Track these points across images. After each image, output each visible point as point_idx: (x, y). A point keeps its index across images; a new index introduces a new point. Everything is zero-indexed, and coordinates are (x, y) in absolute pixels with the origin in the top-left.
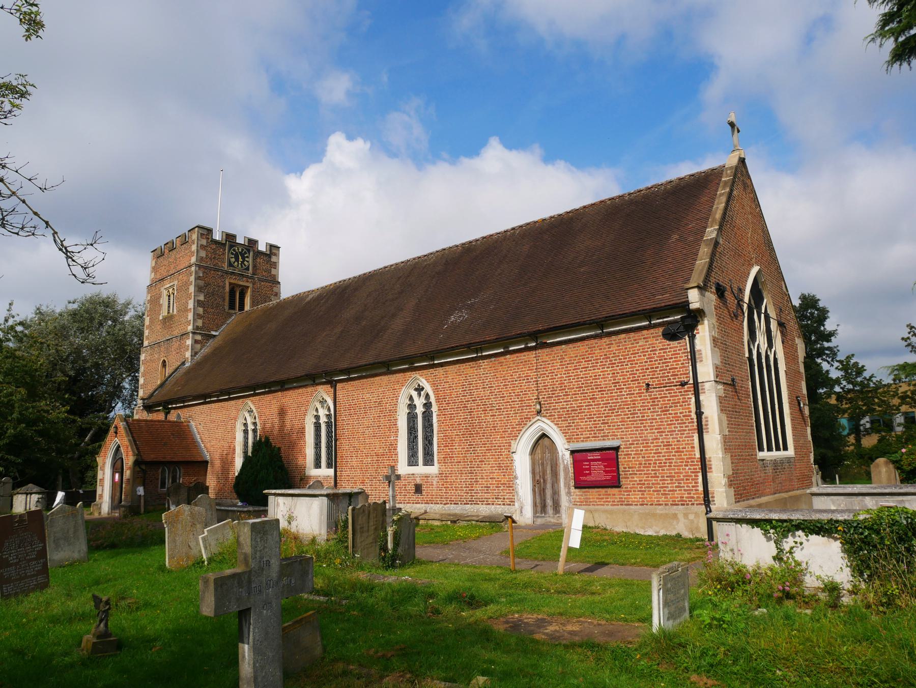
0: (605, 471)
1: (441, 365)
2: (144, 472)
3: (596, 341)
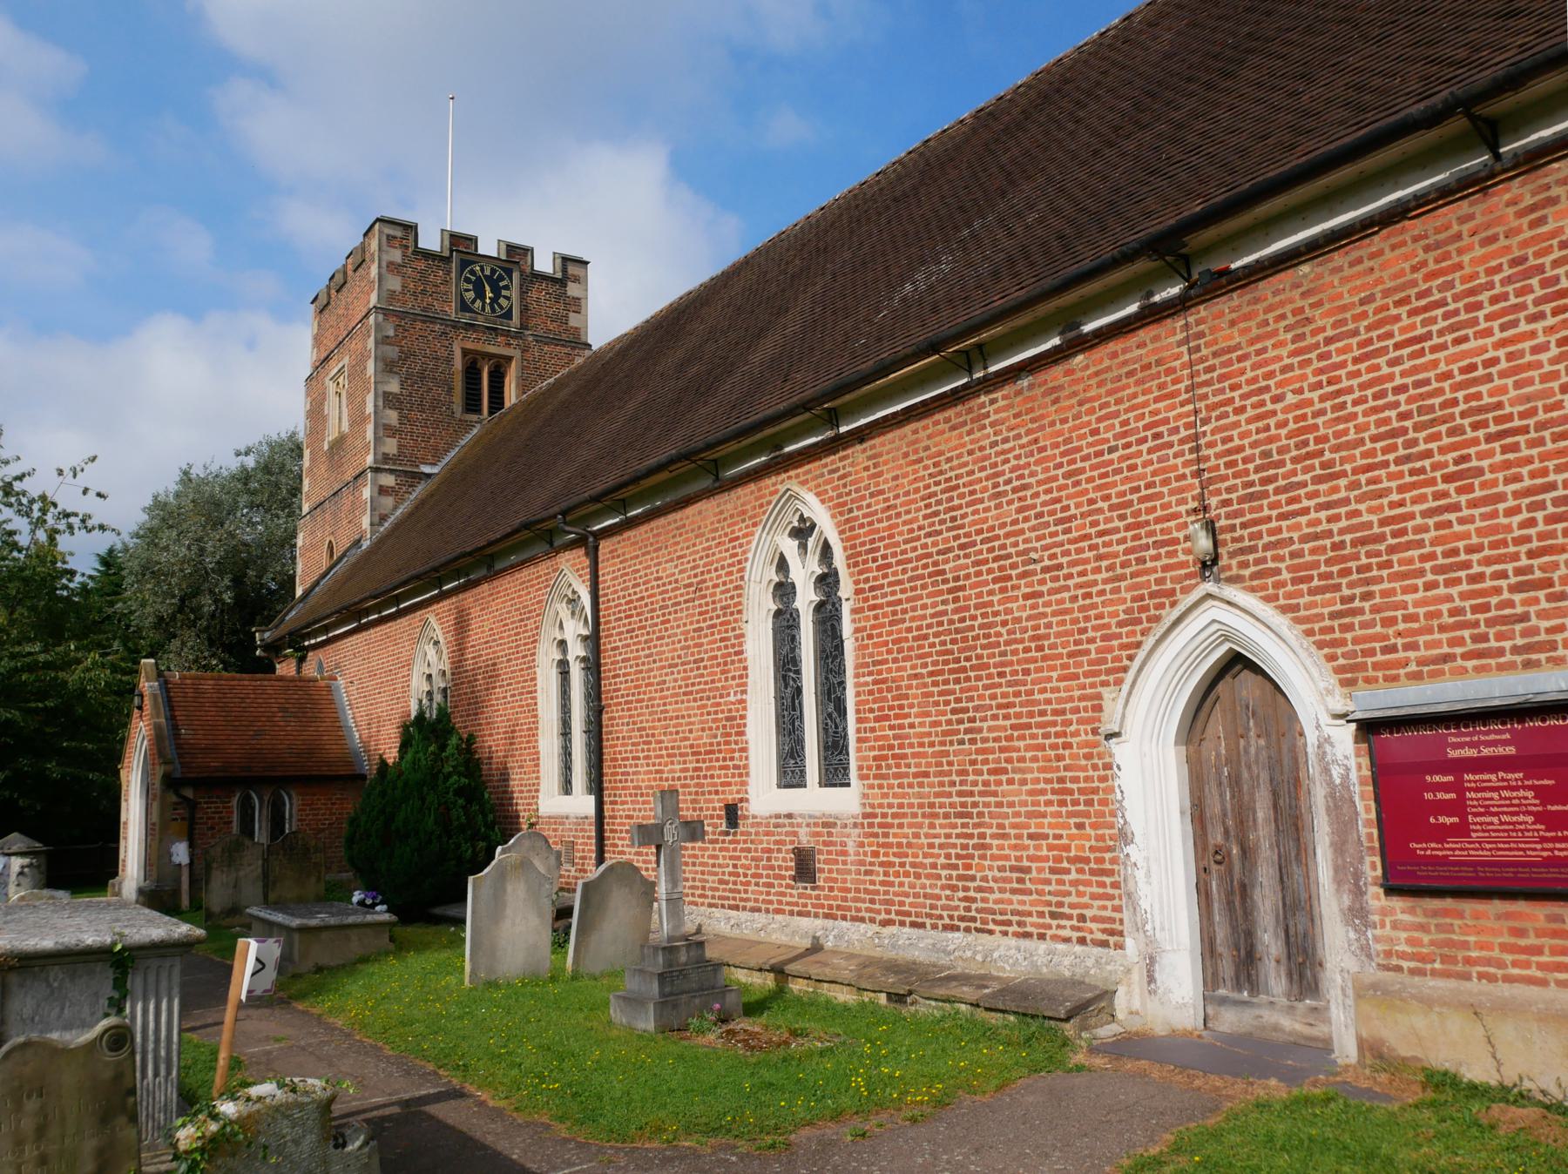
2: (192, 806)
3: (1464, 207)
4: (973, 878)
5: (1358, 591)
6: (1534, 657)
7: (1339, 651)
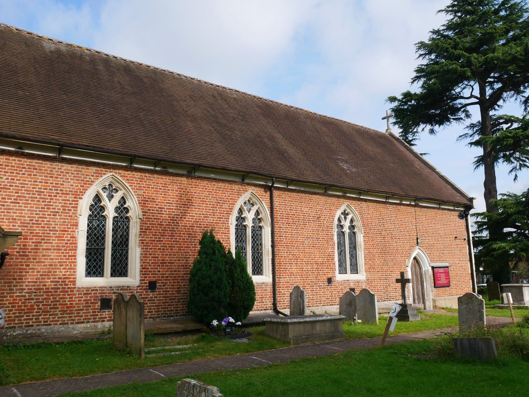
1: (366, 200)
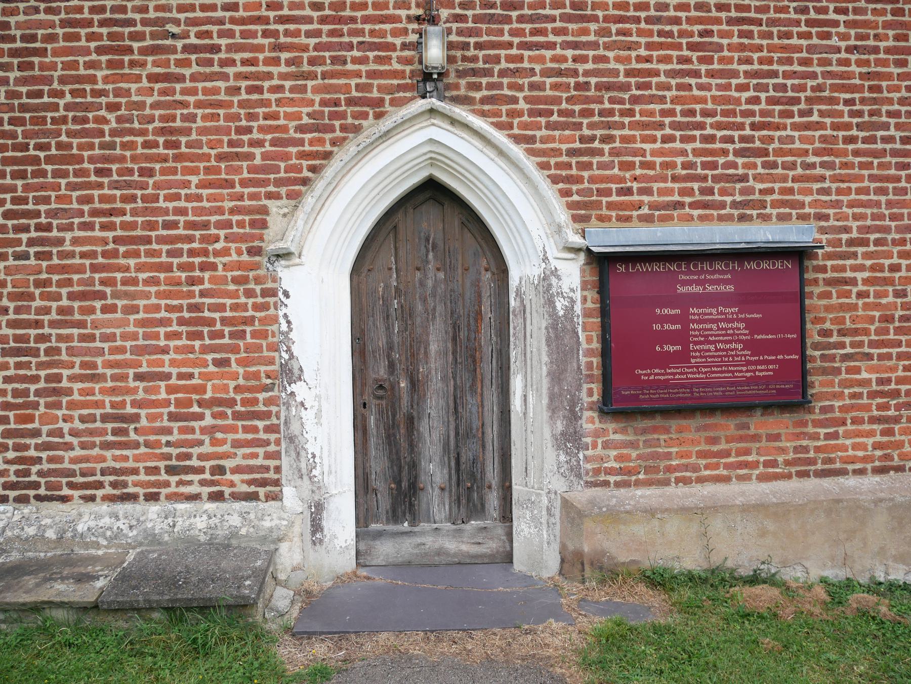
0: (753, 346)
4: (36, 433)
5: (598, 133)
6: (748, 212)
7: (575, 188)
